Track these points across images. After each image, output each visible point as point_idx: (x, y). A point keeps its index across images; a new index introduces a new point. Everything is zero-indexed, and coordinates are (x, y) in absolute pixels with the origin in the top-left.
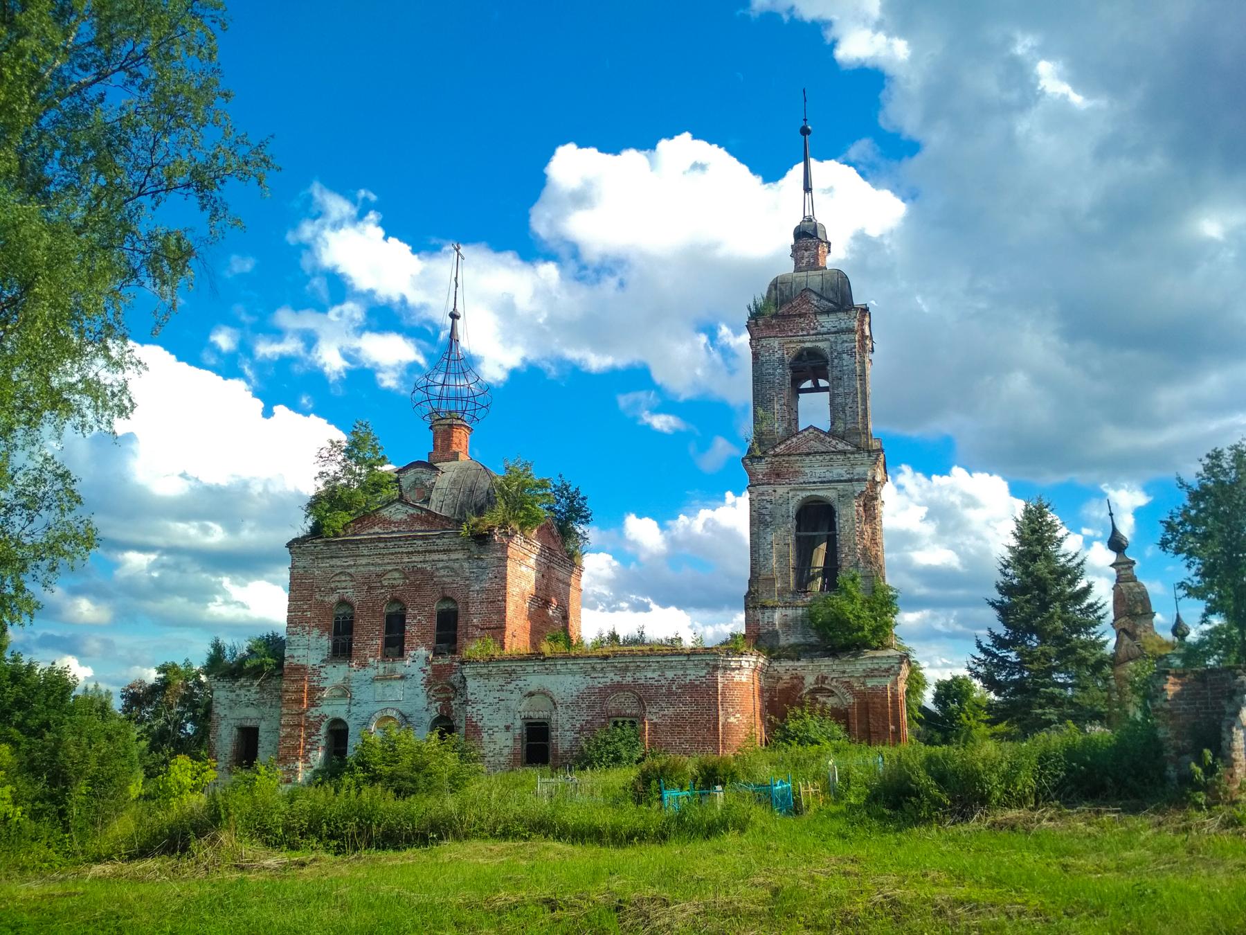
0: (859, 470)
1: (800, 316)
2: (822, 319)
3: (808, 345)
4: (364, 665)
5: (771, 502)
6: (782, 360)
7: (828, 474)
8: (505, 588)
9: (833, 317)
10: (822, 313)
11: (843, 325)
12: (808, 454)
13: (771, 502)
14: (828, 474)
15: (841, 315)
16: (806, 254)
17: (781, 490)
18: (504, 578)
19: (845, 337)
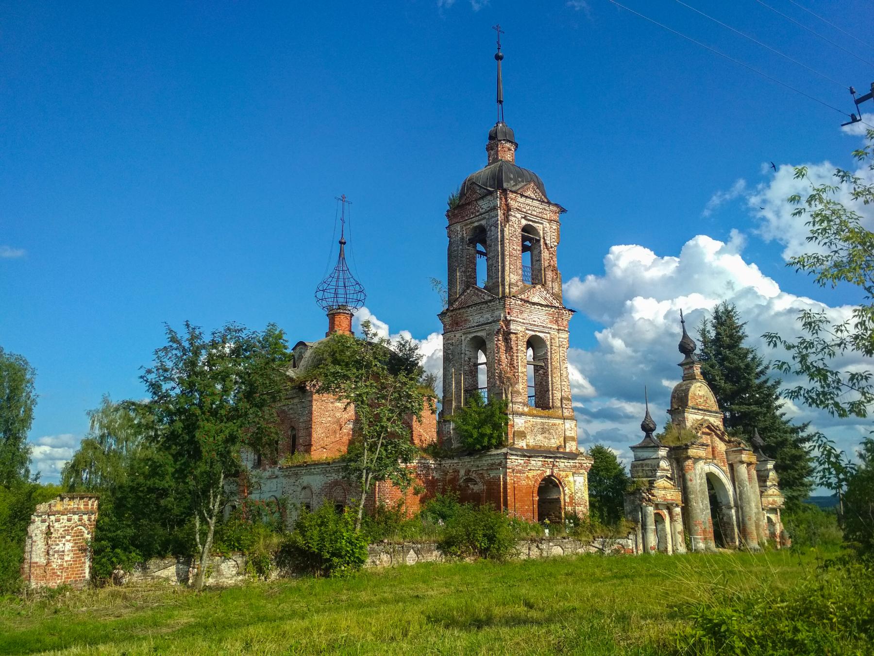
0: (497, 313)
1: (469, 204)
2: (480, 203)
3: (476, 224)
4: (265, 470)
5: (452, 344)
6: (462, 239)
7: (481, 319)
8: (311, 420)
9: (486, 200)
10: (480, 199)
11: (492, 205)
12: (468, 307)
13: (452, 344)
14: (481, 319)
15: (489, 198)
16: (492, 152)
17: (458, 335)
18: (311, 413)
19: (492, 214)
